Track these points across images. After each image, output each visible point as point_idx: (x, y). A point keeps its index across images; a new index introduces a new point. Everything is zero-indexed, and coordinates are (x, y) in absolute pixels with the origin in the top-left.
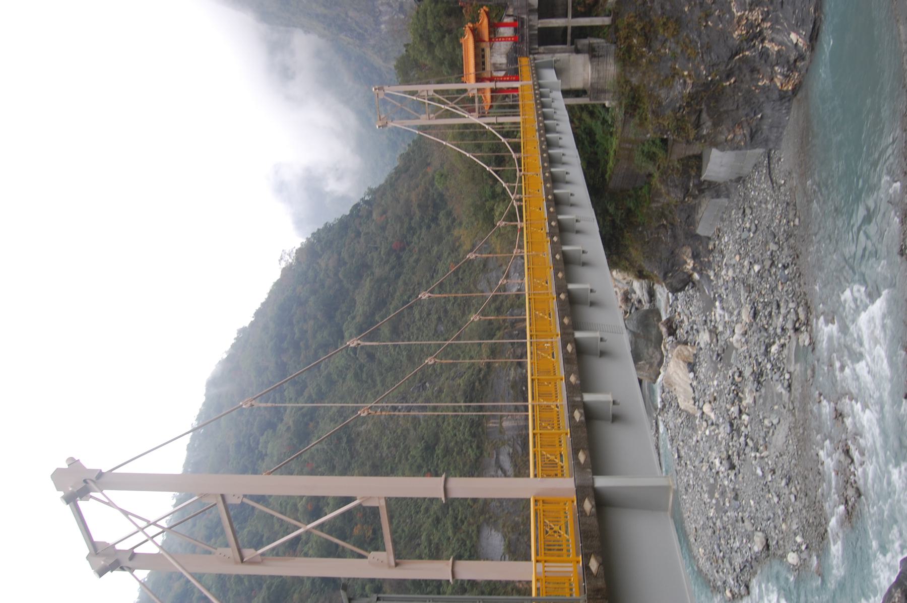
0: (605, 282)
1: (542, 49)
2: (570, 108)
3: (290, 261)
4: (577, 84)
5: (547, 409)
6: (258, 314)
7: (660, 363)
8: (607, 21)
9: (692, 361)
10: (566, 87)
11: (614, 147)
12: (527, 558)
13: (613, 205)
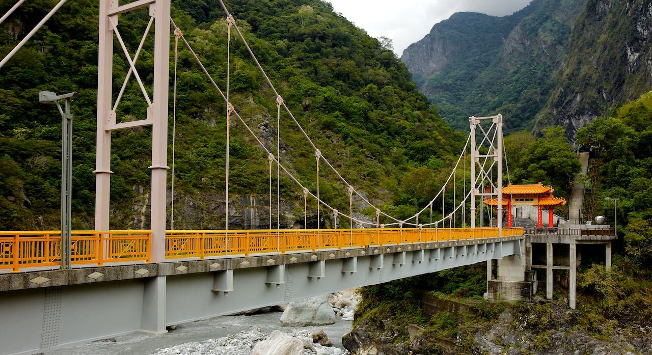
2: (483, 265)
3: (383, 46)
4: (501, 271)
5: (245, 247)
8: (550, 295)
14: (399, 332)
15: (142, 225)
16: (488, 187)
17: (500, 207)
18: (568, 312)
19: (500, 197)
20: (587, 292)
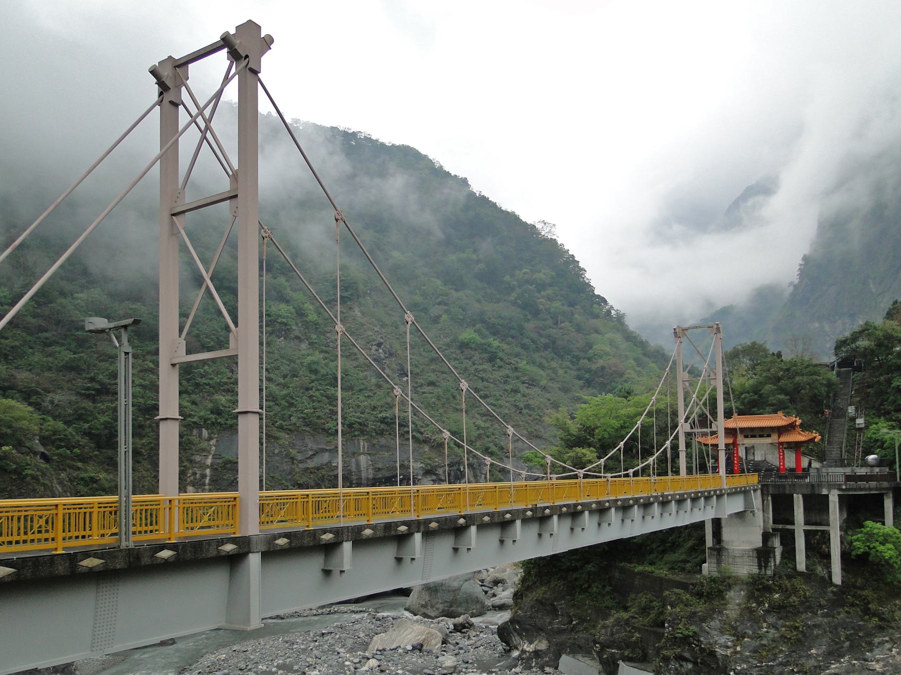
0: (497, 562)
2: (701, 525)
4: (727, 534)
5: (345, 507)
7: (426, 616)
8: (801, 565)
9: (424, 648)
10: (723, 523)
11: (657, 571)
13: (593, 569)
14: (580, 618)
16: (703, 421)
17: (722, 446)
18: (830, 589)
19: (721, 433)
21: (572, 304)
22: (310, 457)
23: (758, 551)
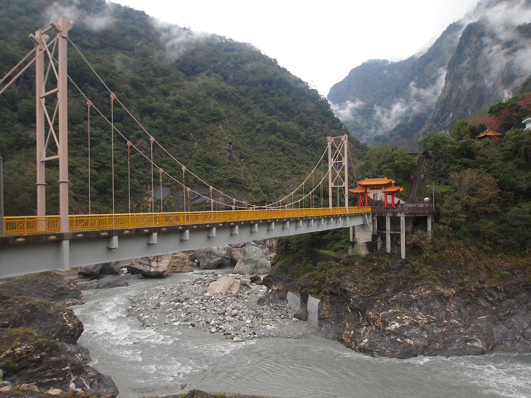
1: (375, 218)
6: (284, 70)
8: (389, 250)
12: (47, 213)
15: (149, 210)
20: (414, 248)
21: (323, 123)
22: (197, 198)
23: (367, 243)
